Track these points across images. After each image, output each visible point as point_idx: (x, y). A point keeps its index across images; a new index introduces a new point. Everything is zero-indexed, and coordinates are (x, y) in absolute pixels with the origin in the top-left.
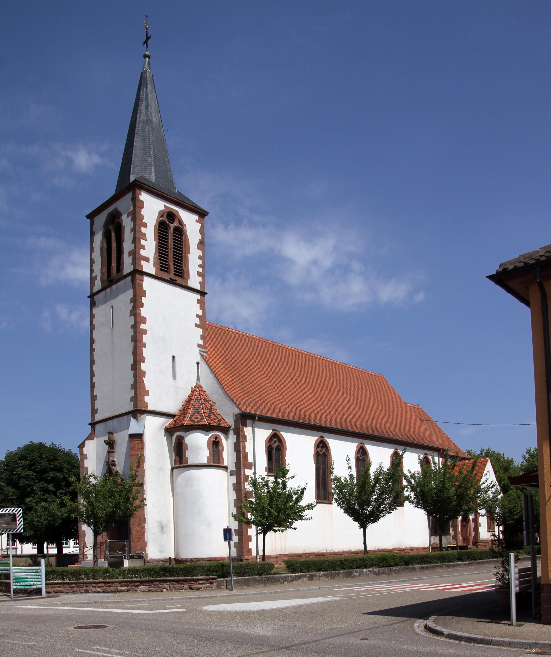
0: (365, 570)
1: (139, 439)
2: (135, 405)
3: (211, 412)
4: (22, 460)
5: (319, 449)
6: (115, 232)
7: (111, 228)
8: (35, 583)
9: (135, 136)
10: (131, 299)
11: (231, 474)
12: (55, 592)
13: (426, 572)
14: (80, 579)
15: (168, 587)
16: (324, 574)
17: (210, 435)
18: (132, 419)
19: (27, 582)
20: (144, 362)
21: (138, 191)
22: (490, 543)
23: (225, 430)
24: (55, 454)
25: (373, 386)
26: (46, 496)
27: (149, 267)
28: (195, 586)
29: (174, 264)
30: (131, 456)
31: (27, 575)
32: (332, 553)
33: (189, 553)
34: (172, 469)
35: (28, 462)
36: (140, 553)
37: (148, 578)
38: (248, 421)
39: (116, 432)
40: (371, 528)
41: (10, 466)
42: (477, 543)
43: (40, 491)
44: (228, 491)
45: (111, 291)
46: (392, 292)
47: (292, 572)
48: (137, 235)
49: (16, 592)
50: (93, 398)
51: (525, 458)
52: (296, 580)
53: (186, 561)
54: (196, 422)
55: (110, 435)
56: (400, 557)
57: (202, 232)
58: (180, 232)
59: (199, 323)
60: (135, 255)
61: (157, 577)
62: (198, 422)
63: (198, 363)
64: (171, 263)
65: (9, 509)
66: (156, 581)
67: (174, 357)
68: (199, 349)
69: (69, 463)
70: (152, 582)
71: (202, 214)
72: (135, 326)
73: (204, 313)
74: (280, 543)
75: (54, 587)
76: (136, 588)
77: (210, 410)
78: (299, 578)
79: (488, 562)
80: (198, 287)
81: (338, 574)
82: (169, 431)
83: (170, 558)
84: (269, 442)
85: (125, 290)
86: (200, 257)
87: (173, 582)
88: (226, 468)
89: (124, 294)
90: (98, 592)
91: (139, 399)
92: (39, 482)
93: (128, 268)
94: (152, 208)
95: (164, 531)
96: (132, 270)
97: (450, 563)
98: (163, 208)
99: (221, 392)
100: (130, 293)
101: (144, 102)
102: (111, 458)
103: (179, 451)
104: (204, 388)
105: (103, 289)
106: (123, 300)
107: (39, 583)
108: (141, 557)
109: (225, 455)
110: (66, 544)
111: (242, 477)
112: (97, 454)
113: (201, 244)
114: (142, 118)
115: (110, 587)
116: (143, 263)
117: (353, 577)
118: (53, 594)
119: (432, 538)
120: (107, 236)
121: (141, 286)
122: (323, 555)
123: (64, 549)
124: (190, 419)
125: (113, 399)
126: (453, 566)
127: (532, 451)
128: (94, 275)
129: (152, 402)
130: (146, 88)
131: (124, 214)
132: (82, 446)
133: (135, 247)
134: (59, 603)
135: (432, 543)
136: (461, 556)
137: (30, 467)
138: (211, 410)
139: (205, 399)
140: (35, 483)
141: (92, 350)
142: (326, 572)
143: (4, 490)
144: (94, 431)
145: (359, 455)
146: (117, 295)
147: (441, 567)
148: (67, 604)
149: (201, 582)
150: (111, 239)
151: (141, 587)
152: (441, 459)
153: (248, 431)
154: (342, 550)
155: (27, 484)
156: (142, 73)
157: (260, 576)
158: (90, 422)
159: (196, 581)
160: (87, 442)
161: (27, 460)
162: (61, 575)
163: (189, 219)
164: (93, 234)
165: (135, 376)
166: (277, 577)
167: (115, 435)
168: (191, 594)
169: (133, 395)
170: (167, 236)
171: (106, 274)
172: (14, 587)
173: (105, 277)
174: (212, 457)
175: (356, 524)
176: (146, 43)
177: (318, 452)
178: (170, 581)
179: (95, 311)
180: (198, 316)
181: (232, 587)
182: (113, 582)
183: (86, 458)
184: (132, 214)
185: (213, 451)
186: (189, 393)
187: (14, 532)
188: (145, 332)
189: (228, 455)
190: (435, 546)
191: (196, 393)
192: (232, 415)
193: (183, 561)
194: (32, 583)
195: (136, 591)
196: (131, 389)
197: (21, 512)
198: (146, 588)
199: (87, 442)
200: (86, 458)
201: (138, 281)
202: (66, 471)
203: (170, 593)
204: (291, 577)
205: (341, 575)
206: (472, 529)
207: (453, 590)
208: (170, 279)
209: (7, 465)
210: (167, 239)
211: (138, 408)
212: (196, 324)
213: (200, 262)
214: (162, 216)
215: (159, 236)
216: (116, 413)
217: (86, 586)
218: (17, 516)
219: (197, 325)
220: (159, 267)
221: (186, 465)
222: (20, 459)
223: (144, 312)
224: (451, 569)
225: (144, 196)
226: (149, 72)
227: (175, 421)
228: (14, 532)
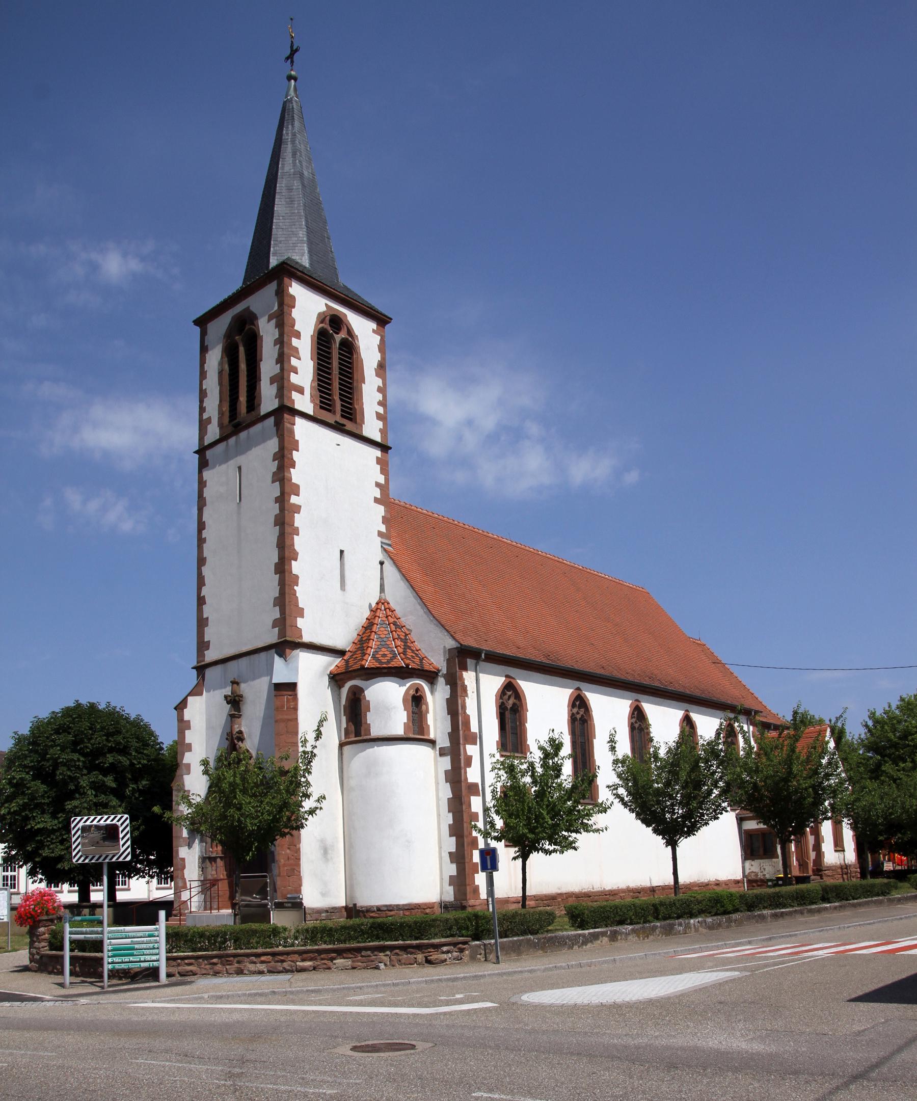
0: (692, 921)
1: (290, 693)
2: (282, 633)
3: (406, 647)
4: (60, 734)
5: (575, 710)
7: (240, 341)
8: (148, 958)
9: (277, 196)
10: (275, 454)
11: (442, 752)
12: (181, 975)
13: (781, 922)
14: (225, 949)
15: (387, 959)
16: (633, 930)
17: (408, 685)
18: (276, 658)
19: (133, 955)
20: (296, 560)
21: (286, 280)
22: (839, 870)
23: (431, 677)
24: (118, 722)
25: (635, 605)
26: (102, 798)
27: (304, 402)
28: (436, 957)
29: (341, 400)
30: (276, 721)
31: (133, 943)
32: (602, 892)
33: (373, 896)
34: (342, 745)
35: (71, 737)
36: (295, 898)
37: (354, 945)
38: (469, 661)
39: (245, 682)
40: (685, 844)
41: (39, 745)
42: (821, 870)
43: (91, 788)
44: (437, 783)
45: (236, 442)
46: (588, 469)
47: (582, 926)
48: (286, 350)
49: (114, 974)
50: (202, 623)
51: (866, 726)
52: (591, 942)
53: (369, 910)
54: (385, 663)
55: (235, 685)
56: (741, 896)
57: (382, 348)
58: (349, 347)
59: (379, 496)
60: (281, 382)
61: (365, 942)
62: (388, 662)
63: (382, 563)
64: (336, 398)
67: (342, 552)
68: (380, 539)
69: (139, 739)
70: (358, 950)
71: (381, 320)
72: (282, 500)
73: (387, 480)
74: (554, 873)
75: (179, 965)
76: (329, 963)
77: (405, 641)
78: (595, 937)
79: (867, 903)
80: (377, 438)
81: (654, 929)
82: (336, 679)
84: (501, 698)
85: (264, 439)
86: (380, 390)
87: (397, 951)
88: (432, 743)
90: (261, 973)
91: (288, 623)
92: (89, 773)
93: (268, 400)
94: (308, 307)
95: (329, 856)
96: (276, 406)
97: (813, 907)
98: (325, 309)
99: (420, 611)
100: (273, 445)
101: (290, 146)
102: (236, 726)
103: (355, 714)
104: (393, 605)
105: (223, 439)
106: (259, 457)
107: (154, 958)
108: (297, 905)
109: (430, 719)
110: (124, 883)
111: (462, 757)
112: (208, 721)
113: (381, 368)
114: (287, 169)
116: (295, 395)
117: (675, 934)
118: (177, 978)
119: (748, 863)
120: (230, 353)
121: (292, 432)
122: (587, 895)
123: (117, 893)
124: (374, 657)
125: (238, 624)
126: (819, 911)
127: (878, 714)
128: (205, 416)
129: (310, 628)
130: (293, 125)
131: (262, 317)
132: (181, 706)
133: (282, 369)
134: (206, 996)
135: (747, 872)
136: (827, 893)
137: (75, 746)
138: (406, 641)
139: (395, 624)
140: (82, 775)
141: (201, 541)
142: (637, 927)
143: (28, 788)
144: (204, 680)
145: (634, 720)
146: (248, 448)
147: (802, 913)
148: (221, 997)
149: (445, 949)
150: (238, 357)
151: (339, 961)
152: (751, 728)
153: (469, 677)
154: (615, 887)
155: (69, 776)
156: (285, 103)
157: (536, 936)
158: (195, 664)
159: (437, 947)
160: (189, 698)
161: (69, 733)
162: (191, 940)
163: (363, 330)
164: (204, 349)
165: (282, 584)
166: (562, 937)
167: (243, 686)
168: (431, 972)
169: (278, 616)
170: (329, 353)
171: (227, 414)
173: (226, 420)
174: (411, 724)
175: (659, 840)
176: (290, 57)
177: (573, 714)
178: (392, 948)
179: (206, 474)
180: (378, 485)
181: (498, 957)
182: (288, 953)
183: (189, 728)
184: (277, 317)
185: (413, 713)
186: (367, 613)
187: (114, 860)
188: (297, 509)
189: (435, 720)
190: (753, 877)
191: (380, 614)
193: (363, 911)
194: (142, 958)
195: (329, 968)
196: (274, 606)
198: (348, 963)
199: (189, 698)
200: (189, 728)
201: (287, 425)
202: (134, 753)
203: (393, 972)
204: (584, 936)
205: (657, 931)
206: (811, 847)
207: (815, 953)
208: (336, 422)
209: (34, 743)
210: (329, 358)
211: (288, 639)
212: (375, 498)
213: (380, 397)
214: (322, 322)
215: (318, 354)
216: (245, 649)
217: (238, 962)
218: (121, 829)
219: (376, 500)
220: (318, 402)
221: (368, 737)
222: (57, 732)
223: (296, 475)
224: (816, 917)
225: (296, 289)
226: (296, 102)
227: (347, 662)
228: (114, 860)
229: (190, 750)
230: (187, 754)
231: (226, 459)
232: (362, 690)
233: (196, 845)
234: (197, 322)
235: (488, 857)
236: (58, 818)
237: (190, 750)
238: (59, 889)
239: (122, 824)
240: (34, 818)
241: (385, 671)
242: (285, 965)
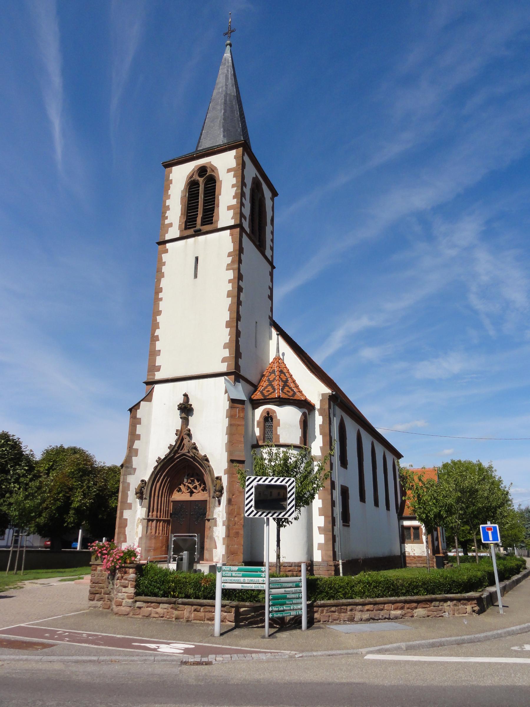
65: (282, 478)
66: (436, 600)
107: (275, 609)
148: (441, 645)
183: (140, 423)
197: (294, 484)
200: (140, 423)
218: (288, 490)
235: (490, 532)
239: (289, 486)
241: (292, 401)
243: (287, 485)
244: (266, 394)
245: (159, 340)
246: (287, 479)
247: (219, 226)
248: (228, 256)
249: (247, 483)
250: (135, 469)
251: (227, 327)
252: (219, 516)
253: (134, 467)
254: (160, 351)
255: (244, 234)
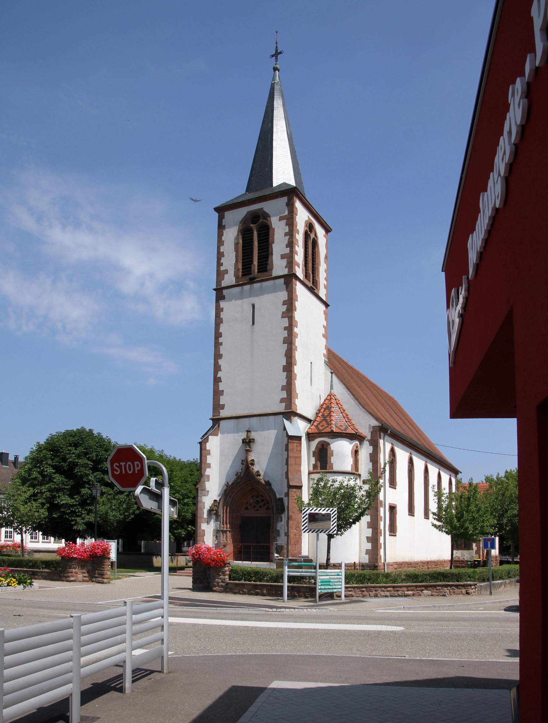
1: (298, 442)
4: (72, 446)
6: (257, 231)
8: (336, 587)
66: (439, 586)
70: (435, 586)
71: (327, 230)
83: (355, 563)
89: (273, 294)
90: (387, 596)
93: (279, 267)
100: (284, 295)
106: (270, 301)
107: (339, 587)
115: (398, 591)
120: (245, 234)
128: (222, 268)
148: (429, 607)
158: (211, 417)
172: (320, 591)
178: (451, 586)
192: (368, 427)
198: (429, 592)
203: (454, 597)
216: (256, 412)
217: (376, 591)
218: (332, 516)
229: (210, 467)
230: (208, 470)
231: (241, 297)
232: (328, 444)
233: (212, 523)
234: (217, 209)
235: (489, 543)
236: (74, 499)
237: (210, 467)
238: (49, 541)
240: (59, 496)
242: (399, 593)
243: (331, 513)
244: (321, 428)
245: (221, 382)
246: (331, 509)
247: (274, 274)
248: (283, 305)
249: (303, 512)
250: (208, 491)
251: (284, 371)
252: (281, 529)
253: (207, 490)
254: (223, 391)
255: (298, 204)
